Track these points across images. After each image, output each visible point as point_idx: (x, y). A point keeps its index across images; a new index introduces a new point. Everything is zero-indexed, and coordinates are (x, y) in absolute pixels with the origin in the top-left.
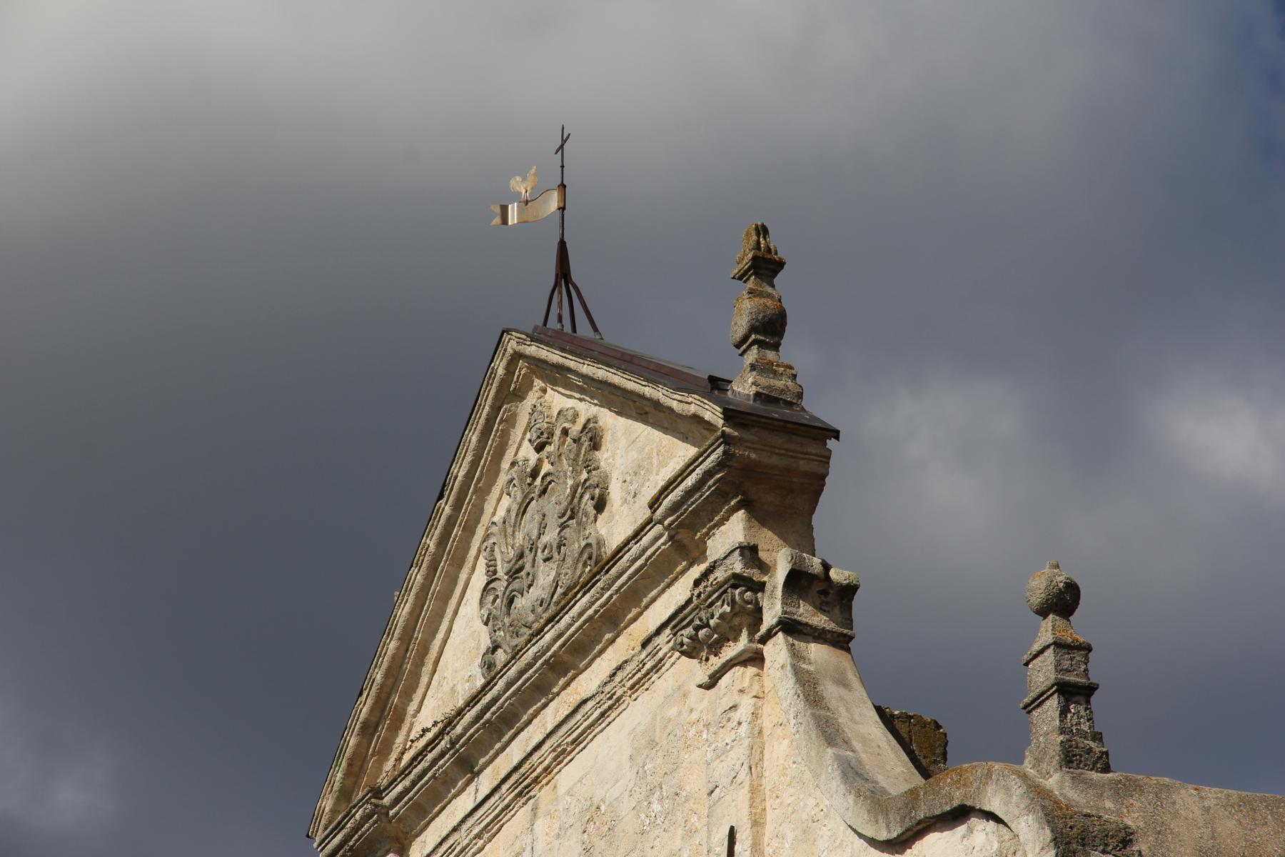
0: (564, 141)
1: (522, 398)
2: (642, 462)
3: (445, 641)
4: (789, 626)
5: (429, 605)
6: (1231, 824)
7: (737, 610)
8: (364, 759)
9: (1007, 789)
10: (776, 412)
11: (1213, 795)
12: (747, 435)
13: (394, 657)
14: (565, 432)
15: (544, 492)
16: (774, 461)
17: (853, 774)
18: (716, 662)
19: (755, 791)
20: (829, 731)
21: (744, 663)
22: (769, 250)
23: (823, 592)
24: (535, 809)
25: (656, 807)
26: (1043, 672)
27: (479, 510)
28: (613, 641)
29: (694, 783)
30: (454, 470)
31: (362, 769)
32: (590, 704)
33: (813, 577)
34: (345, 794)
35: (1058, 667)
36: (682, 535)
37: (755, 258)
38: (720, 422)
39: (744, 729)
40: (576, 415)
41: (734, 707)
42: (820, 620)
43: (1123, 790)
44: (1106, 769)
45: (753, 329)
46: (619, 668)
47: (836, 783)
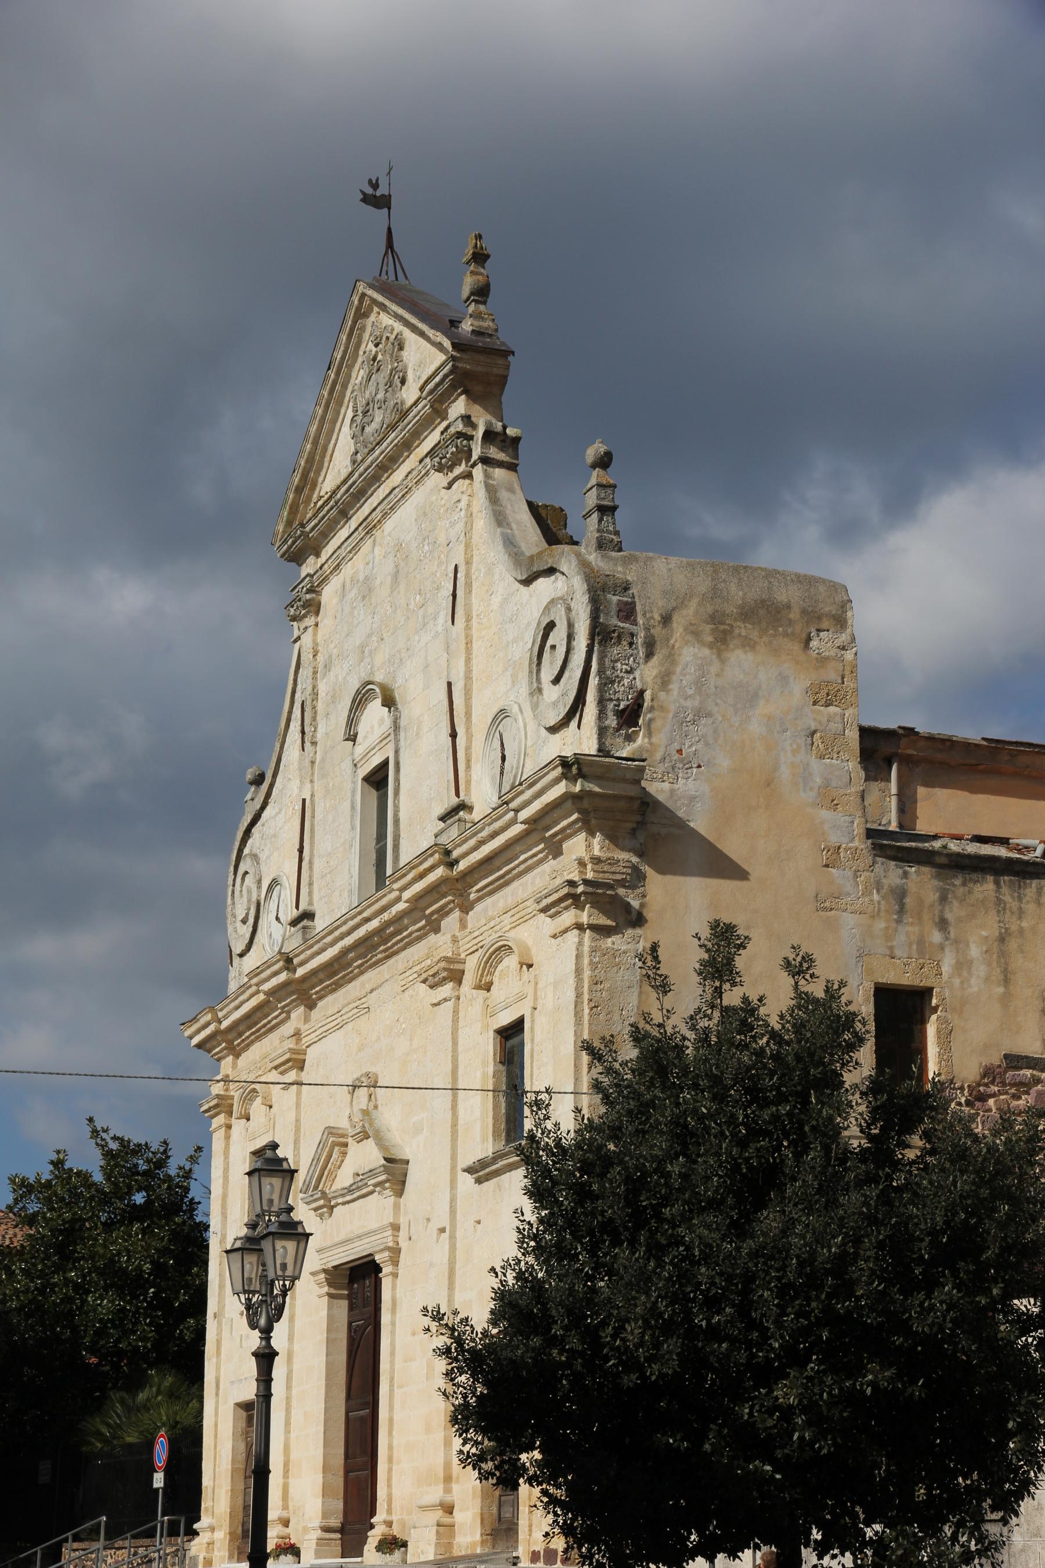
0: (390, 169)
1: (368, 317)
2: (424, 357)
3: (335, 445)
4: (485, 460)
5: (326, 426)
6: (681, 577)
7: (459, 451)
8: (298, 506)
9: (570, 562)
10: (481, 342)
11: (674, 560)
12: (465, 356)
13: (309, 453)
14: (388, 338)
15: (378, 370)
16: (479, 369)
17: (509, 543)
18: (451, 476)
19: (468, 546)
20: (500, 518)
21: (464, 478)
22: (482, 248)
23: (503, 441)
24: (374, 541)
25: (426, 548)
26: (592, 499)
27: (349, 377)
28: (408, 456)
29: (442, 539)
30: (335, 354)
31: (297, 511)
32: (397, 490)
33: (497, 434)
34: (289, 523)
35: (598, 497)
36: (437, 405)
37: (474, 254)
38: (450, 349)
39: (463, 513)
40: (393, 329)
41: (459, 501)
42: (501, 456)
43: (628, 561)
44: (620, 550)
45: (472, 294)
46: (409, 473)
47: (501, 547)
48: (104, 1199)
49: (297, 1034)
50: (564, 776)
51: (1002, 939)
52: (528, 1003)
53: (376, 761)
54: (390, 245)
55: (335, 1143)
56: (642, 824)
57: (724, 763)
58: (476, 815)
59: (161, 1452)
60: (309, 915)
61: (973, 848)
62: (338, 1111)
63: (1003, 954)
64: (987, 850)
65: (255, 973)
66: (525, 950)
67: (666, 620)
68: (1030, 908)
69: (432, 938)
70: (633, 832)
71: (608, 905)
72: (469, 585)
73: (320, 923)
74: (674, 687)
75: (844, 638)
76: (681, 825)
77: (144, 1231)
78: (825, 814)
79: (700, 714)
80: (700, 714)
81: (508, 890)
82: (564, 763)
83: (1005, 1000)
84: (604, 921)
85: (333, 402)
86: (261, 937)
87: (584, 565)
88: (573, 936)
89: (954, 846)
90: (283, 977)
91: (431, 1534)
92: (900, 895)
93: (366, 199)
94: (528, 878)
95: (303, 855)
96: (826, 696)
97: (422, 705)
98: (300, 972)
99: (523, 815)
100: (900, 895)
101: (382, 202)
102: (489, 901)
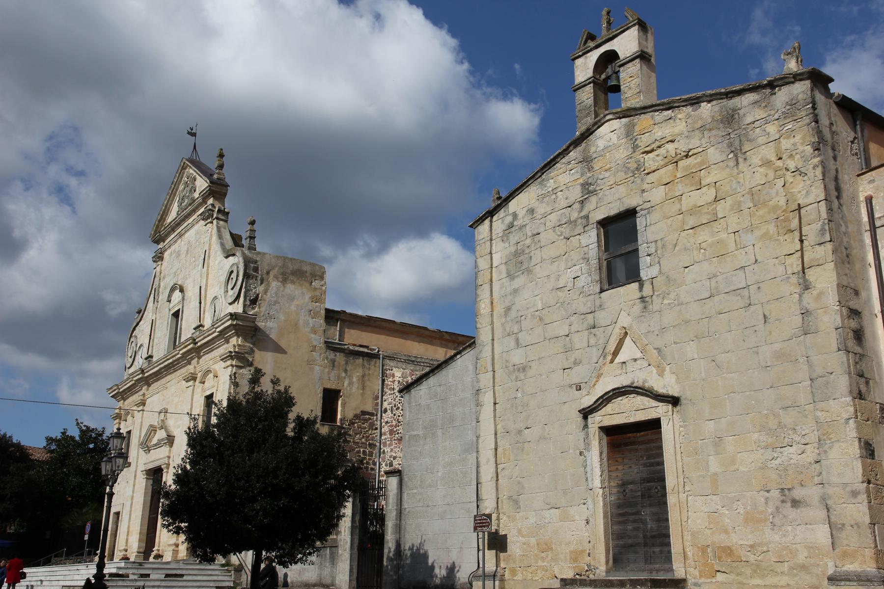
2: (202, 184)
4: (217, 218)
17: (222, 245)
19: (210, 244)
20: (220, 237)
26: (248, 234)
42: (223, 218)
48: (78, 445)
49: (144, 394)
50: (231, 319)
51: (363, 376)
52: (215, 388)
53: (176, 309)
55: (153, 430)
56: (254, 335)
57: (282, 318)
59: (88, 528)
60: (151, 357)
61: (357, 349)
62: (155, 420)
63: (363, 381)
64: (361, 349)
66: (216, 372)
67: (268, 273)
68: (372, 367)
69: (189, 366)
70: (252, 338)
71: (240, 358)
72: (209, 256)
73: (154, 359)
74: (269, 294)
76: (268, 336)
77: (91, 457)
78: (313, 336)
79: (276, 302)
80: (276, 302)
82: (231, 314)
83: (363, 394)
84: (240, 364)
85: (173, 195)
86: (136, 363)
87: (243, 254)
89: (351, 348)
91: (171, 553)
92: (333, 361)
93: (189, 133)
95: (153, 339)
96: (316, 299)
97: (192, 293)
98: (146, 375)
99: (218, 330)
100: (333, 361)
101: (194, 135)
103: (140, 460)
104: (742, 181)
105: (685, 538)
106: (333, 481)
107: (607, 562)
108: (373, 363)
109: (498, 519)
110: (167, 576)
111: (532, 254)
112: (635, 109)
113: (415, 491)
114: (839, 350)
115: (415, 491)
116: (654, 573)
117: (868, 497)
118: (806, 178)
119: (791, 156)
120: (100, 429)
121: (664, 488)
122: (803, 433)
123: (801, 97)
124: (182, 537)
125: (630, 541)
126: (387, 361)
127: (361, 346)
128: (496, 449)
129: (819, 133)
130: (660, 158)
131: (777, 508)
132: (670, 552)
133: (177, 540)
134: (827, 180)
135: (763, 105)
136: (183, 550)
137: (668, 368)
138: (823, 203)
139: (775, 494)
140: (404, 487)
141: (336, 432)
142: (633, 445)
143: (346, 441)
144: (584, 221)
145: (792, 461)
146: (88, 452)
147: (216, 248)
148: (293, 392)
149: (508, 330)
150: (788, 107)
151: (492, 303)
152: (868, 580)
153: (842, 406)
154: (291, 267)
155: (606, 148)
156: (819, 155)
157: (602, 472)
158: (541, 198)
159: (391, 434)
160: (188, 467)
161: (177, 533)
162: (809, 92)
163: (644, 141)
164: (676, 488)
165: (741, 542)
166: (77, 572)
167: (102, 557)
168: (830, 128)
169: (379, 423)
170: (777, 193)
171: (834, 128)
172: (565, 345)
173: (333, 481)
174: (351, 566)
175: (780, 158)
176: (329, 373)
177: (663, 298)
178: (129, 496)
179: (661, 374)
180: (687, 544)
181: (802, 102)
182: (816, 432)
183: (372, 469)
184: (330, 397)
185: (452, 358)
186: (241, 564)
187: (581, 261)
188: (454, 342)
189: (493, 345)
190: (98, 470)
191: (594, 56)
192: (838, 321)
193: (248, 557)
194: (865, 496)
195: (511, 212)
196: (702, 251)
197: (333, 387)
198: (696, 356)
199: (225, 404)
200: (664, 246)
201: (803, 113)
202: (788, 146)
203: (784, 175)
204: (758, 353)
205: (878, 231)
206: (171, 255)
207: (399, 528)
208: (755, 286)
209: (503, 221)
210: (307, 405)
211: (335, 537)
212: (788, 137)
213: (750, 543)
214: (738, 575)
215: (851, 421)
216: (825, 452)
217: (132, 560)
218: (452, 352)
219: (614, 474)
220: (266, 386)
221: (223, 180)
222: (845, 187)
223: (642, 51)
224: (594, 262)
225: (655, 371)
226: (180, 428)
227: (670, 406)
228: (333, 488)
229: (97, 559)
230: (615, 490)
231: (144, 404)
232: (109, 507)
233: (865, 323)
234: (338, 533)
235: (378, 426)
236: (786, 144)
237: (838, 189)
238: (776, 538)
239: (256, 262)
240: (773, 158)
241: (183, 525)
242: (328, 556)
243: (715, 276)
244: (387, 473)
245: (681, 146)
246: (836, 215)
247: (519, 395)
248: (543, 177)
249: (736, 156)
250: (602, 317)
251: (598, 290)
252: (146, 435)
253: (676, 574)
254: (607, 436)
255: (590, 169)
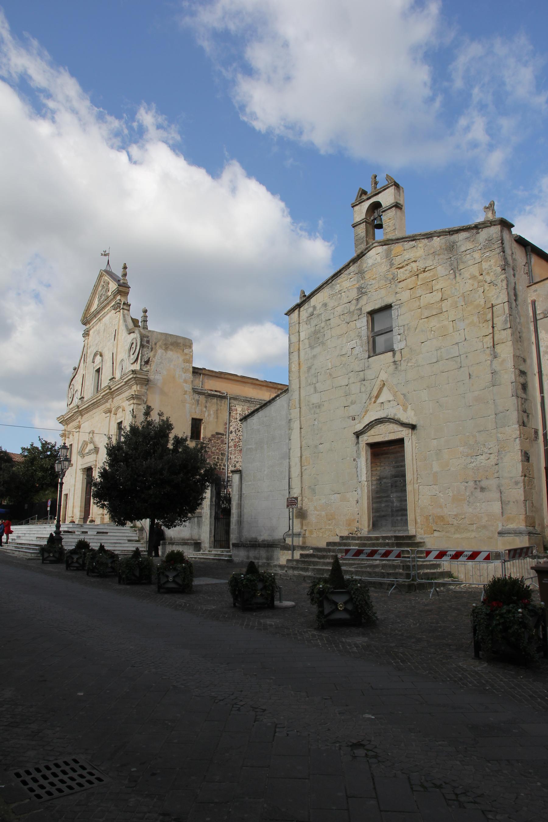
2: (113, 286)
4: (123, 309)
17: (126, 326)
19: (119, 326)
20: (125, 321)
48: (41, 452)
49: (79, 422)
51: (217, 410)
53: (98, 367)
54: (108, 263)
55: (85, 444)
58: (116, 380)
59: (49, 503)
60: (83, 398)
61: (213, 393)
62: (86, 438)
63: (217, 413)
65: (72, 408)
67: (156, 344)
68: (223, 405)
73: (85, 399)
74: (156, 357)
75: (191, 350)
77: (49, 460)
78: (185, 384)
79: (161, 363)
80: (161, 363)
81: (121, 395)
82: (133, 371)
83: (217, 422)
86: (74, 402)
88: (132, 405)
89: (209, 392)
90: (77, 410)
91: (99, 519)
92: (198, 401)
94: (125, 393)
97: (108, 357)
98: (80, 409)
99: (124, 381)
102: (117, 397)
103: (78, 463)
104: (458, 288)
105: (416, 511)
106: (198, 477)
107: (369, 526)
108: (223, 402)
109: (302, 500)
110: (98, 533)
111: (325, 333)
112: (392, 240)
113: (250, 483)
114: (513, 396)
115: (250, 483)
116: (397, 532)
117: (524, 485)
118: (496, 287)
119: (488, 273)
120: (53, 443)
121: (405, 481)
122: (489, 447)
123: (494, 236)
124: (106, 511)
125: (383, 513)
126: (232, 401)
127: (216, 391)
128: (301, 457)
129: (505, 259)
130: (408, 272)
131: (472, 493)
132: (407, 520)
133: (103, 511)
134: (509, 289)
135: (472, 240)
136: (107, 518)
137: (409, 407)
138: (506, 304)
139: (471, 484)
140: (243, 481)
141: (199, 446)
142: (386, 453)
143: (206, 451)
144: (359, 312)
145: (482, 464)
146: (47, 457)
147: (122, 328)
148: (172, 421)
149: (309, 381)
150: (487, 242)
151: (299, 364)
152: (520, 533)
153: (512, 430)
154: (170, 340)
155: (373, 265)
156: (505, 273)
157: (367, 471)
158: (331, 296)
159: (235, 447)
160: (108, 468)
161: (103, 507)
162: (499, 233)
163: (397, 261)
164: (412, 481)
165: (450, 513)
166: (44, 529)
167: (59, 521)
168: (512, 257)
169: (227, 440)
170: (479, 296)
171: (514, 256)
172: (345, 392)
173: (198, 477)
174: (210, 528)
175: (482, 274)
176: (195, 409)
177: (408, 362)
178: (72, 485)
179: (405, 410)
180: (417, 514)
181: (495, 239)
182: (497, 446)
183: (223, 469)
184: (196, 424)
185: (274, 399)
186: (142, 527)
187: (357, 338)
188: (275, 388)
189: (300, 391)
190: (53, 468)
191: (366, 205)
192: (513, 378)
193: (146, 523)
194: (522, 484)
195: (312, 305)
196: (433, 332)
197: (198, 417)
198: (427, 399)
199: (128, 429)
200: (409, 329)
201: (496, 246)
202: (487, 267)
203: (484, 285)
204: (464, 398)
205: (538, 322)
206: (94, 332)
207: (240, 506)
208: (465, 355)
209: (307, 311)
210: (181, 429)
211: (200, 511)
212: (486, 261)
213: (455, 513)
214: (446, 532)
215: (518, 440)
216: (502, 458)
217: (77, 523)
218: (273, 395)
219: (374, 473)
220: (155, 417)
221: (127, 284)
222: (519, 294)
223: (397, 202)
224: (365, 338)
225: (401, 408)
226: (102, 443)
227: (410, 431)
228: (199, 481)
229: (55, 522)
230: (375, 483)
231: (80, 428)
232: (61, 491)
233: (529, 379)
234: (202, 508)
235: (227, 442)
236: (485, 265)
237: (515, 295)
238: (471, 510)
239: (148, 337)
240: (477, 274)
241: (106, 503)
242: (196, 522)
243: (440, 348)
244: (233, 472)
245: (421, 265)
246: (514, 312)
247: (316, 423)
248: (333, 283)
249: (454, 272)
250: (369, 374)
251: (367, 357)
252: (81, 447)
253: (410, 532)
254: (371, 449)
255: (363, 278)
